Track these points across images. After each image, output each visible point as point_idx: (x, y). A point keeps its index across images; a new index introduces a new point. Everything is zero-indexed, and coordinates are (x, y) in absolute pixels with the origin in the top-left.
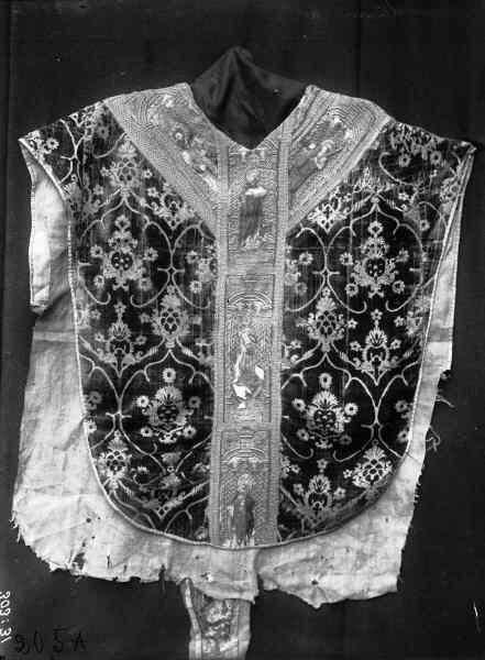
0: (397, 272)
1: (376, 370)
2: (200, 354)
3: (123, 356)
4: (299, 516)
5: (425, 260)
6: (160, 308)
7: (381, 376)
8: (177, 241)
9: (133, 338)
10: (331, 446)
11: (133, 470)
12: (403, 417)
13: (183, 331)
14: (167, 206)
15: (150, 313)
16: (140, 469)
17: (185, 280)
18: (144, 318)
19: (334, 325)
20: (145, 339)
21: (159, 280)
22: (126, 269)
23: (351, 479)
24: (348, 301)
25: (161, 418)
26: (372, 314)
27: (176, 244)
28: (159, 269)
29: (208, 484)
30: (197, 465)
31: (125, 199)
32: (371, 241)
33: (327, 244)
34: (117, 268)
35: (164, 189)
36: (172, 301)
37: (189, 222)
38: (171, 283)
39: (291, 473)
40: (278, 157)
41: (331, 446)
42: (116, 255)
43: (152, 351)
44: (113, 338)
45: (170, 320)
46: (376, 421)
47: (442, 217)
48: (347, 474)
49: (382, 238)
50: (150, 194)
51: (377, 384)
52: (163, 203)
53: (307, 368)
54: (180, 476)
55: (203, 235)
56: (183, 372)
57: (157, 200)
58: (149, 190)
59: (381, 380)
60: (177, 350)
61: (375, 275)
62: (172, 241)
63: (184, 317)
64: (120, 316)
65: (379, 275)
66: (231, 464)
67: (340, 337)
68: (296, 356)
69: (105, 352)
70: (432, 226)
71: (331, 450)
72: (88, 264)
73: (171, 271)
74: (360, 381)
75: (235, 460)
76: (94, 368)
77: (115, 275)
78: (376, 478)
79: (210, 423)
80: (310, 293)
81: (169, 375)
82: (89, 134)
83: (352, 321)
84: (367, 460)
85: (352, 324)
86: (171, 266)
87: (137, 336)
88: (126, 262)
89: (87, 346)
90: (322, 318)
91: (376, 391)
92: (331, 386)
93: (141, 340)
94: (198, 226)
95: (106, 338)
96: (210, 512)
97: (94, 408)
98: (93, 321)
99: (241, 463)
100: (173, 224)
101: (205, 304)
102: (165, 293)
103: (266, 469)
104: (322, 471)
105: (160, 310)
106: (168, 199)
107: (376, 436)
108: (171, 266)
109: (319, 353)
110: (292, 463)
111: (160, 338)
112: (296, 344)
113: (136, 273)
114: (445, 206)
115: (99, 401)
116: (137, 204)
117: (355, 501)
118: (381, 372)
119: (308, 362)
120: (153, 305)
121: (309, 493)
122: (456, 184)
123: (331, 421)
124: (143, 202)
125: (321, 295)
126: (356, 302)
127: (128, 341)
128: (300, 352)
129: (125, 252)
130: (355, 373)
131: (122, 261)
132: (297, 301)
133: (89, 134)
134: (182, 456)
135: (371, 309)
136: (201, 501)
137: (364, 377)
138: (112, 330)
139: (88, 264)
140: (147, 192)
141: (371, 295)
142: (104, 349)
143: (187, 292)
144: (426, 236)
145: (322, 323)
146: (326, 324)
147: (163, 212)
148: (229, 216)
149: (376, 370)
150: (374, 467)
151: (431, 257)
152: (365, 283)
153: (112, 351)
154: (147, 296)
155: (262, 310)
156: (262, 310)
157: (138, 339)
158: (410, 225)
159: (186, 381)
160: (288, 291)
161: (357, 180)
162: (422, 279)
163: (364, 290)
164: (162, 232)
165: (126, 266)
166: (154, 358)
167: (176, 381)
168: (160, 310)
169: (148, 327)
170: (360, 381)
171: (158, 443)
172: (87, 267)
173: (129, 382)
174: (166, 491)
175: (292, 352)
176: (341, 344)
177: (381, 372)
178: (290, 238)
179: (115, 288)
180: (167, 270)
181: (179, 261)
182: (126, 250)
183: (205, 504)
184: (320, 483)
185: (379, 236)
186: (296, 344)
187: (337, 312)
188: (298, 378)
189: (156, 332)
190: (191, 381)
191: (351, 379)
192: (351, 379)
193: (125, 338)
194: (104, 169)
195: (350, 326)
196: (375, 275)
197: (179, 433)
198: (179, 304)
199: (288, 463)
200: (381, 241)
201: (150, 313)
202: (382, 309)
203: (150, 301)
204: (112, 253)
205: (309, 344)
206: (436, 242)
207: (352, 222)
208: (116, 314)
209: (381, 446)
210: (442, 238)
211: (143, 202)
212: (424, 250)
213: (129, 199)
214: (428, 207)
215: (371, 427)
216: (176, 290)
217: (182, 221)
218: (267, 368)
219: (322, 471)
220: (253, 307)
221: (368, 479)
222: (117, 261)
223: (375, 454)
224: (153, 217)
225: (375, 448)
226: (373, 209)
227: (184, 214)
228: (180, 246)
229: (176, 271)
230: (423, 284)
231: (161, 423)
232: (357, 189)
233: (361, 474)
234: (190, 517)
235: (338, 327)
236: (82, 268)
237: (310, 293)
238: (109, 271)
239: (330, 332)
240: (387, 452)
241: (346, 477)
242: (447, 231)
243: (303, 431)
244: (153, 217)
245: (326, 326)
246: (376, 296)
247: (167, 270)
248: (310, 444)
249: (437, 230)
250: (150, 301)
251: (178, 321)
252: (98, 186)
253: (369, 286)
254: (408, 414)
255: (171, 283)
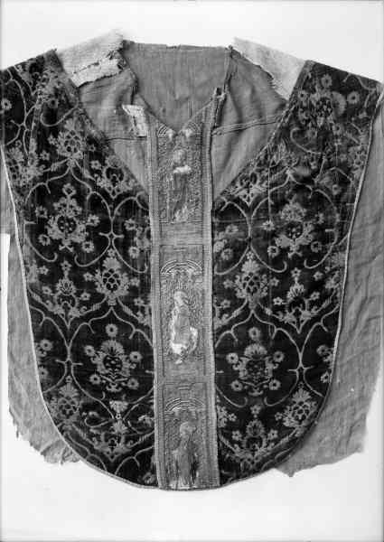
0: (315, 234)
1: (298, 319)
2: (139, 313)
3: (69, 309)
4: (237, 461)
5: (338, 220)
6: (102, 269)
7: (302, 325)
8: (117, 209)
9: (78, 294)
10: (261, 392)
11: (84, 414)
12: (326, 360)
13: (122, 291)
14: (108, 177)
15: (93, 273)
16: (91, 413)
17: (124, 246)
18: (87, 276)
19: (259, 285)
20: (88, 295)
21: (101, 244)
22: (70, 232)
23: (281, 421)
24: (270, 262)
25: (107, 368)
26: (292, 272)
27: (116, 211)
28: (101, 234)
29: (153, 435)
30: (143, 417)
31: (70, 169)
32: (63, 200)
33: (250, 216)
34: (62, 231)
35: (107, 162)
36: (113, 262)
37: (128, 194)
38: (111, 247)
39: (229, 422)
40: (202, 138)
41: (261, 392)
42: (62, 218)
43: (96, 307)
44: (60, 292)
45: (112, 281)
46: (301, 365)
47: (353, 183)
48: (278, 416)
49: (297, 204)
50: (93, 167)
51: (299, 332)
52: (104, 175)
53: (236, 325)
54: (127, 425)
55: (140, 206)
56: (124, 328)
57: (99, 172)
58: (93, 162)
59: (303, 328)
60: (118, 308)
61: (294, 236)
62: (112, 209)
63: (124, 279)
64: (296, 279)
65: (297, 236)
66: (174, 414)
67: (265, 294)
68: (227, 315)
69: (54, 304)
70: (344, 191)
71: (262, 397)
72: (32, 223)
73: (111, 236)
74: (285, 332)
75: (176, 410)
76: (44, 318)
77: (61, 237)
78: (304, 417)
79: (151, 377)
80: (235, 258)
81: (112, 330)
82: (40, 103)
83: (274, 279)
84: (295, 402)
85: (275, 282)
86: (112, 232)
87: (82, 292)
88: (70, 226)
89: (37, 298)
90: (247, 279)
91: (300, 340)
92: (260, 339)
93: (86, 296)
94: (135, 199)
95: (54, 292)
96: (156, 460)
97: (45, 354)
98: (41, 277)
99: (181, 412)
100: (114, 193)
101: (143, 269)
102: (106, 256)
103: (204, 417)
104: (255, 416)
105: (102, 270)
106: (109, 171)
107: (301, 379)
108: (112, 232)
109: (247, 310)
110: (229, 412)
111: (103, 296)
112: (226, 303)
113: (79, 236)
114: (356, 174)
115: (49, 348)
116: (81, 175)
117: (286, 440)
118: (302, 321)
119: (237, 319)
120: (96, 266)
121: (247, 437)
122: (363, 153)
123: (261, 369)
124: (86, 174)
125: (246, 259)
126: (277, 262)
127: (74, 296)
128: (229, 311)
129: (70, 217)
130: (279, 323)
131: (67, 224)
132: (227, 264)
133: (40, 103)
134: (130, 406)
135: (291, 268)
136: (147, 449)
137: (287, 326)
138: (59, 285)
139: (32, 223)
140: (90, 164)
141: (290, 255)
142: (52, 301)
143: (126, 255)
144: (338, 199)
145: (247, 282)
146: (251, 284)
147: (104, 183)
148: (159, 193)
149: (298, 319)
150: (301, 408)
151: (343, 218)
152: (284, 245)
153: (60, 304)
154: (91, 256)
155: (193, 276)
156: (193, 276)
157: (82, 296)
158: (278, 453)
159: (127, 336)
160: (217, 257)
161: (272, 156)
162: (336, 240)
163: (284, 251)
164: (104, 201)
165: (71, 229)
166: (98, 313)
167: (118, 335)
168: (102, 270)
169: (92, 285)
170: (285, 332)
171: (106, 392)
172: (32, 226)
173: (76, 332)
174: (115, 436)
175: (223, 312)
176: (266, 301)
177: (302, 321)
178: (215, 213)
179: (61, 248)
180: (107, 235)
181: (119, 227)
182: (71, 215)
183: (152, 452)
184: (255, 427)
185: (72, 197)
186: (226, 303)
187: (261, 272)
188: (230, 334)
189: (99, 290)
190: (131, 337)
191: (276, 330)
192: (276, 330)
193: (72, 294)
194: (51, 137)
195: (273, 284)
196: (294, 236)
197: (123, 384)
198: (119, 267)
199: (225, 413)
200: (73, 202)
201: (93, 273)
202: (301, 267)
203: (93, 262)
204: (57, 217)
205: (236, 302)
206: (348, 204)
207: (269, 192)
208: (62, 271)
209: (306, 389)
210: (353, 201)
211: (86, 174)
212: (338, 211)
213: (74, 169)
214: (339, 173)
215: (296, 370)
216: (116, 254)
217: (122, 192)
218: (200, 328)
219: (255, 416)
220: (185, 274)
221: (297, 419)
222: (62, 225)
223: (302, 396)
224: (96, 188)
225: (301, 390)
226: (287, 180)
227: (123, 186)
228: (119, 214)
229: (116, 236)
230: (337, 243)
231: (107, 372)
232: (274, 163)
233: (290, 415)
234: (138, 464)
235: (262, 285)
236: (27, 226)
237: (235, 258)
238: (54, 231)
239: (255, 290)
240: (312, 394)
241: (277, 419)
242: (358, 195)
243: (236, 382)
244: (96, 188)
245: (254, 283)
246: (295, 256)
247: (107, 235)
248: (244, 393)
249: (348, 194)
250: (93, 262)
251: (118, 282)
252: (44, 152)
253: (288, 248)
254: (329, 357)
255: (111, 247)
